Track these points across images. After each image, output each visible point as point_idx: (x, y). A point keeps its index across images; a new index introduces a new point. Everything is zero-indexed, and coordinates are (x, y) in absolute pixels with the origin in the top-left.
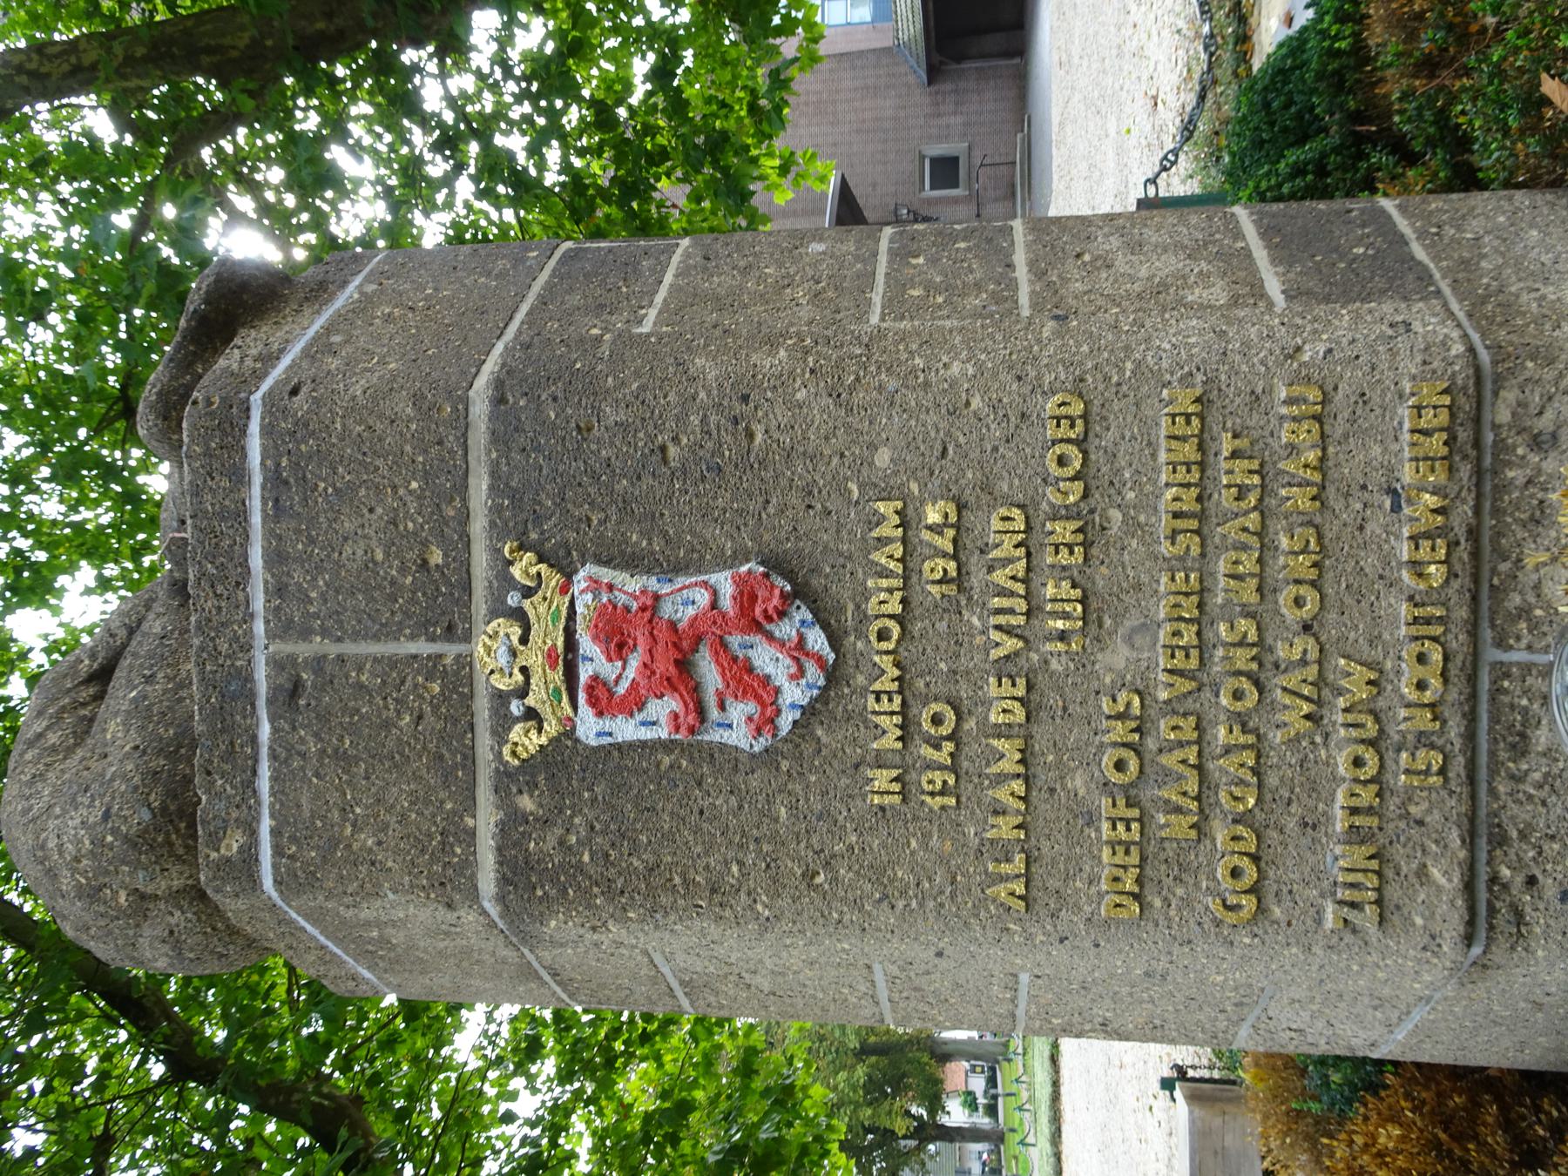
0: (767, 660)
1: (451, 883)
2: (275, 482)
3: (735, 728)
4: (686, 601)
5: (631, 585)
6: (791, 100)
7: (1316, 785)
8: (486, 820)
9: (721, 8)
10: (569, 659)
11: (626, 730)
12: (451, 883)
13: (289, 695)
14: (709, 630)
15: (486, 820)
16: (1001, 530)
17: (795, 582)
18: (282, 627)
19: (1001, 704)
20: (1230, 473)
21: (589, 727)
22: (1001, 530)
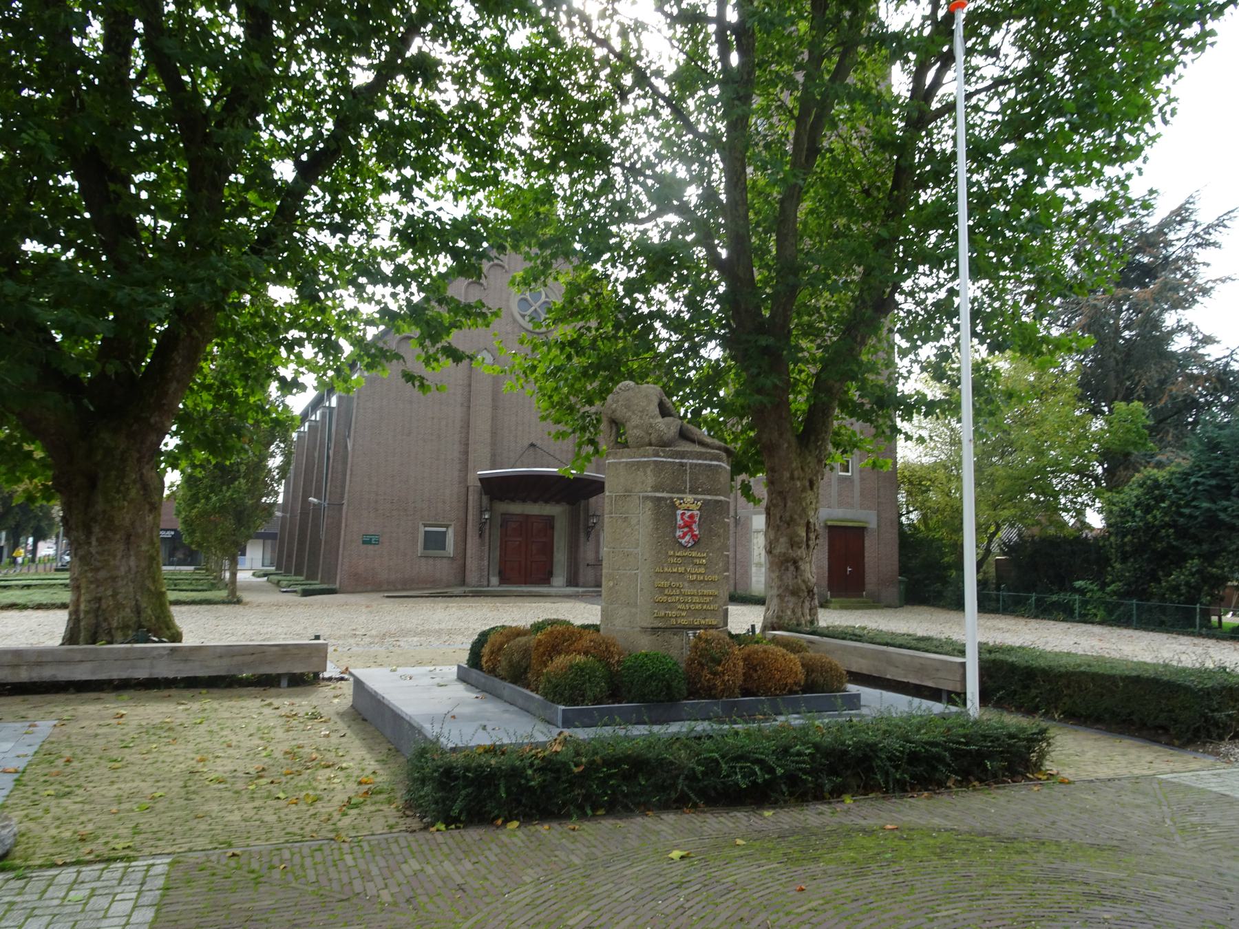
0: (687, 538)
1: (656, 488)
2: (710, 466)
3: (679, 533)
4: (695, 527)
5: (697, 519)
6: (466, 329)
7: (671, 609)
8: (664, 495)
9: (841, 4)
10: (688, 510)
11: (679, 518)
12: (656, 488)
13: (682, 465)
14: (691, 530)
15: (664, 495)
16: (702, 570)
17: (697, 542)
18: (691, 464)
19: (681, 569)
20: (708, 599)
21: (679, 512)
22: (702, 570)
